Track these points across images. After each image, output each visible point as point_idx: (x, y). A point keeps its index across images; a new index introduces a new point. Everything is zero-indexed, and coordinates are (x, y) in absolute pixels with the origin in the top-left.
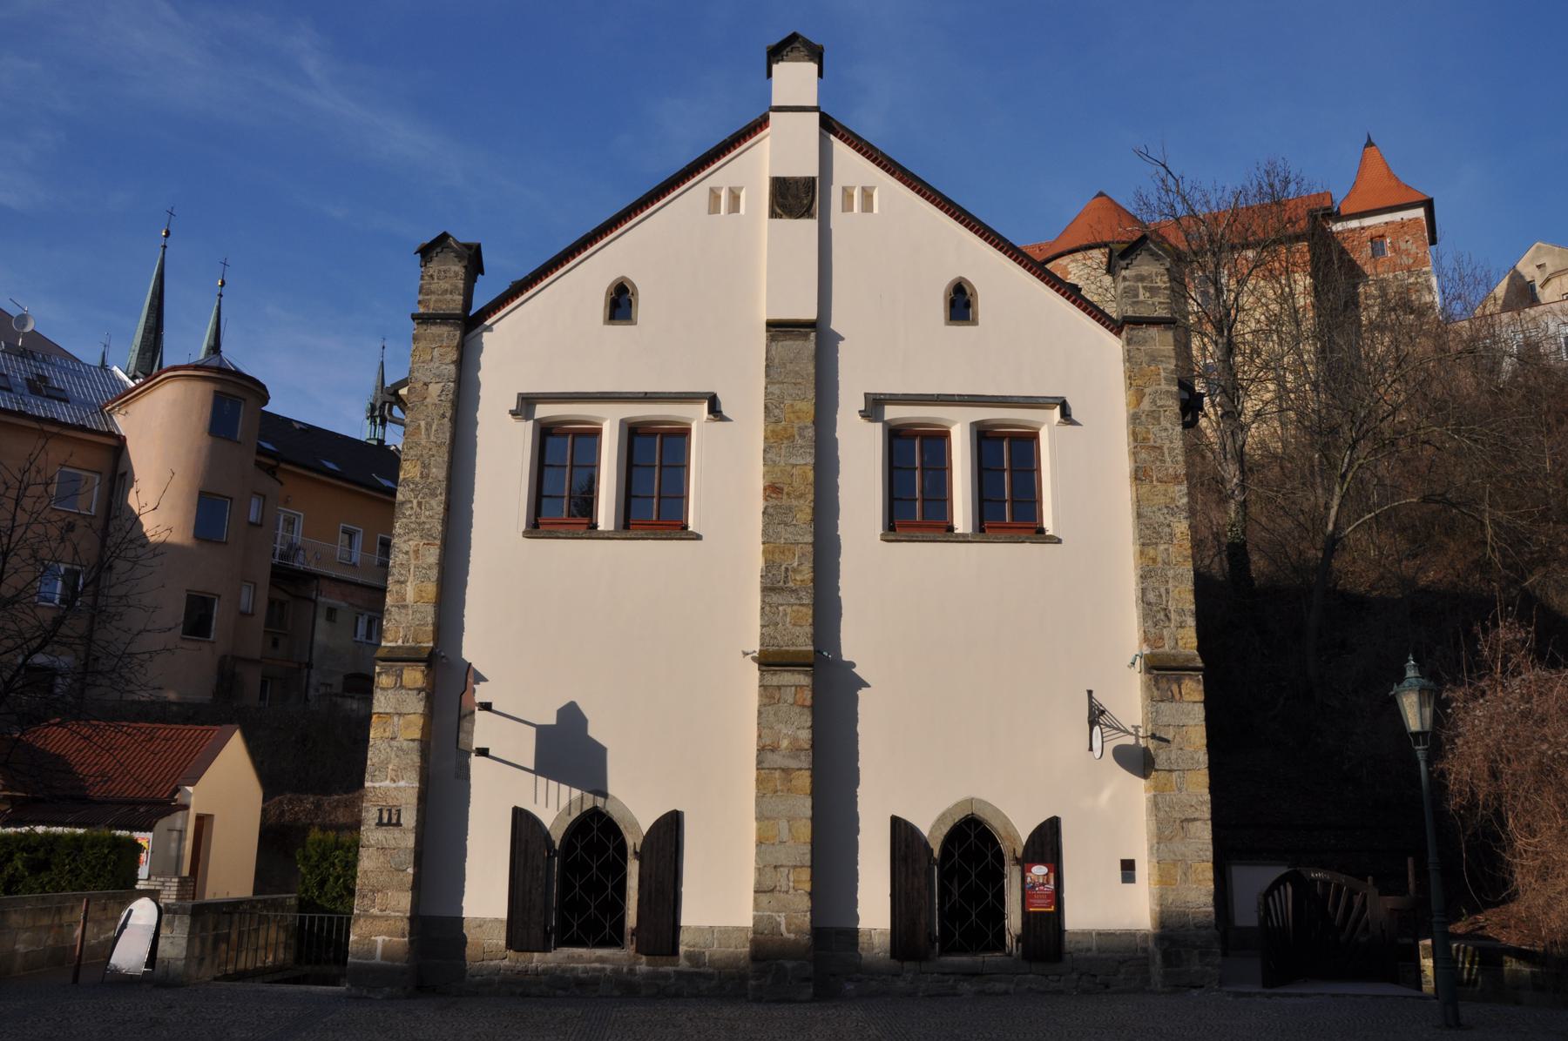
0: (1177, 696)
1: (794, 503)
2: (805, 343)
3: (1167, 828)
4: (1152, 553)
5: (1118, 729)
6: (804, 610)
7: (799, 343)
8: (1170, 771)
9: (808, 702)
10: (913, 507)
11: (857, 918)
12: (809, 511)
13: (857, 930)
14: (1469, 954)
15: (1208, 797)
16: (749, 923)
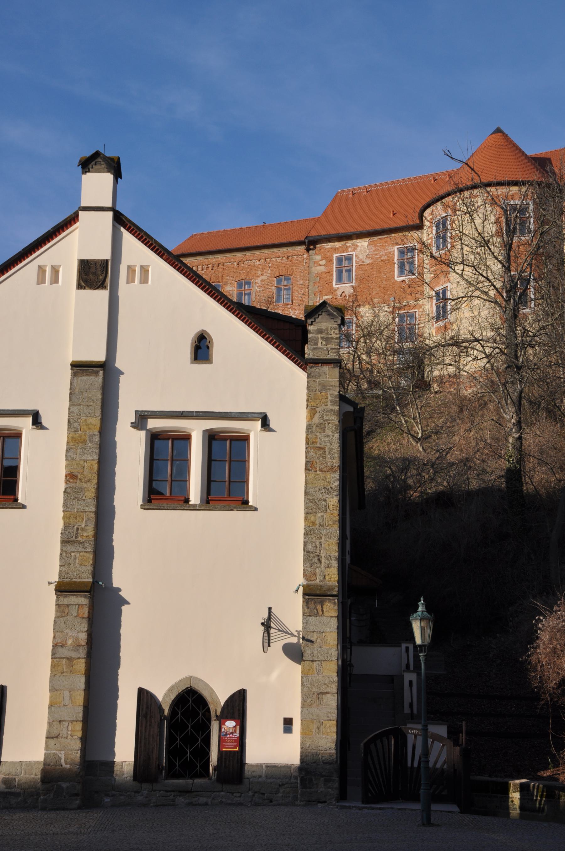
0: (320, 613)
1: (84, 485)
2: (99, 377)
3: (310, 697)
4: (313, 519)
5: (287, 633)
6: (87, 555)
7: (92, 378)
8: (313, 661)
9: (86, 615)
10: (162, 490)
11: (114, 754)
12: (93, 490)
13: (113, 763)
14: (540, 790)
15: (336, 679)
16: (41, 758)
